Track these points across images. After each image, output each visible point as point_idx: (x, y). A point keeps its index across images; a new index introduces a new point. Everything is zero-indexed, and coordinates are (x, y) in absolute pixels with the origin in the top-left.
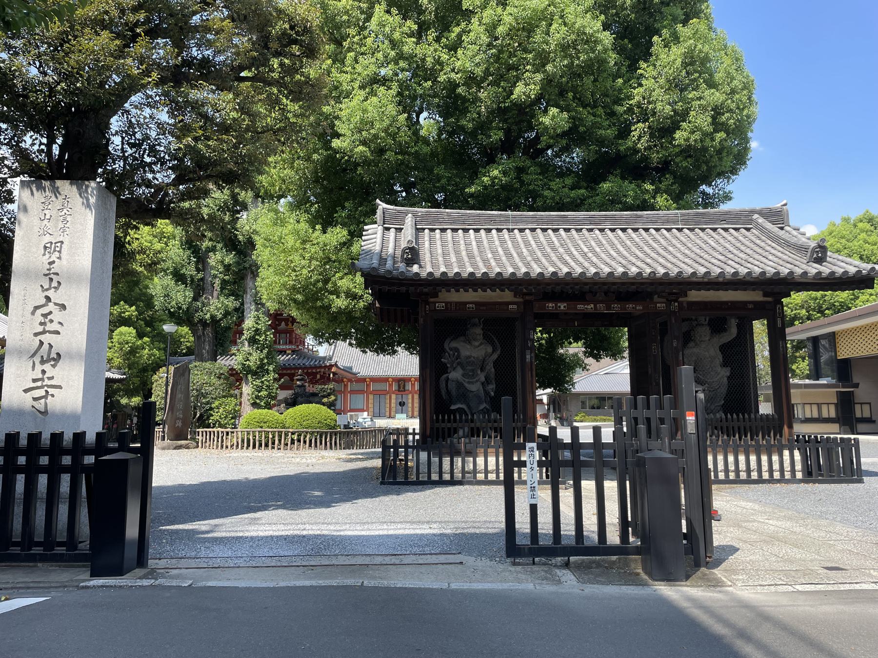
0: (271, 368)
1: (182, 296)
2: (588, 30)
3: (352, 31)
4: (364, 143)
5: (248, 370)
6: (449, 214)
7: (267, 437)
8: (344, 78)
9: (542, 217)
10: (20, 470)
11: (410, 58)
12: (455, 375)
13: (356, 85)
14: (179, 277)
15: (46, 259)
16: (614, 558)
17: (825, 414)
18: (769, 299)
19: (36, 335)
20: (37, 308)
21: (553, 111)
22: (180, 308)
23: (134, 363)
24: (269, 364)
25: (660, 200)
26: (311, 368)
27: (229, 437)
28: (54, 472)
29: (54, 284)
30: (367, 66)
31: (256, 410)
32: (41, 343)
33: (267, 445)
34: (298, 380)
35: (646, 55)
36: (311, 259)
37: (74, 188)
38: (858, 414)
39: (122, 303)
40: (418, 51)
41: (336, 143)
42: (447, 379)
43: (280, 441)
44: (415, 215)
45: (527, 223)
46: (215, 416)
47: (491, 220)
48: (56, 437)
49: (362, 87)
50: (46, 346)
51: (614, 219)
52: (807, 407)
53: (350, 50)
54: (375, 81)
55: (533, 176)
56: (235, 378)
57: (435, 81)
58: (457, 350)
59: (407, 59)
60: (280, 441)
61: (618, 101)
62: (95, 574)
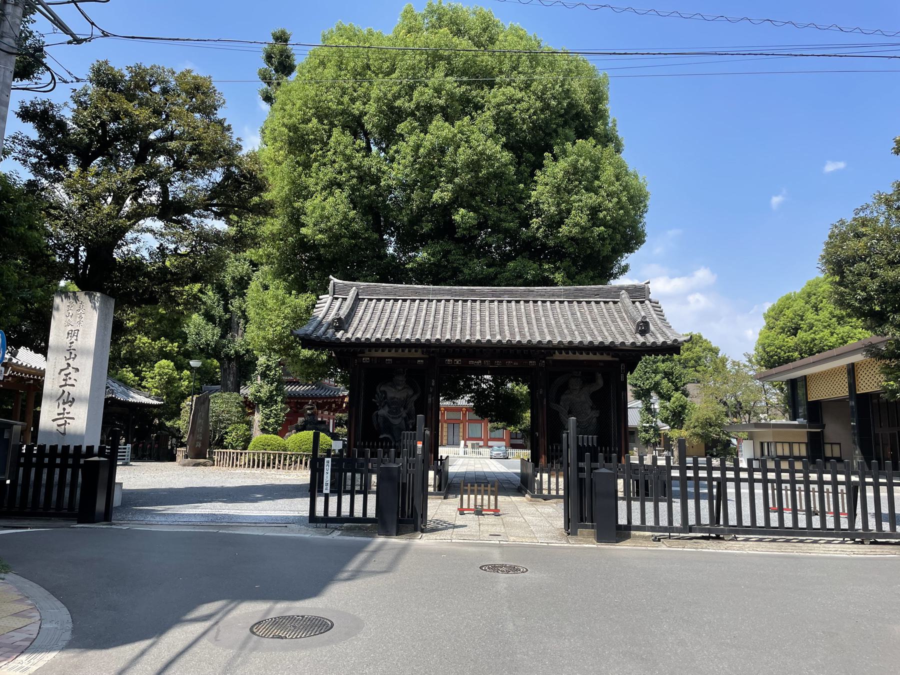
0: (279, 399)
1: (211, 333)
2: (488, 152)
3: (317, 147)
4: (321, 232)
5: (259, 400)
6: (384, 288)
7: (268, 458)
8: (311, 181)
9: (456, 291)
10: (46, 466)
11: (358, 168)
12: (383, 412)
13: (319, 188)
14: (209, 317)
15: (68, 341)
16: (369, 525)
17: (796, 453)
18: (617, 359)
19: (61, 386)
20: (62, 370)
21: (462, 211)
22: (208, 345)
23: (171, 392)
24: (278, 395)
25: (559, 277)
26: (327, 398)
27: (243, 457)
28: (63, 467)
29: (73, 356)
30: (328, 173)
31: (265, 435)
32: (64, 392)
33: (269, 465)
34: (309, 409)
35: (541, 166)
36: (285, 318)
37: (87, 297)
38: (828, 454)
39: (163, 338)
40: (365, 163)
41: (303, 231)
42: (377, 415)
43: (280, 461)
44: (358, 287)
45: (444, 295)
46: (228, 439)
47: (416, 292)
48: (66, 448)
49: (324, 189)
50: (66, 394)
51: (511, 293)
52: (779, 446)
53: (315, 160)
54: (333, 184)
55: (456, 257)
56: (249, 406)
57: (378, 185)
58: (385, 392)
59: (356, 169)
60: (280, 461)
61: (521, 200)
62: (79, 523)
